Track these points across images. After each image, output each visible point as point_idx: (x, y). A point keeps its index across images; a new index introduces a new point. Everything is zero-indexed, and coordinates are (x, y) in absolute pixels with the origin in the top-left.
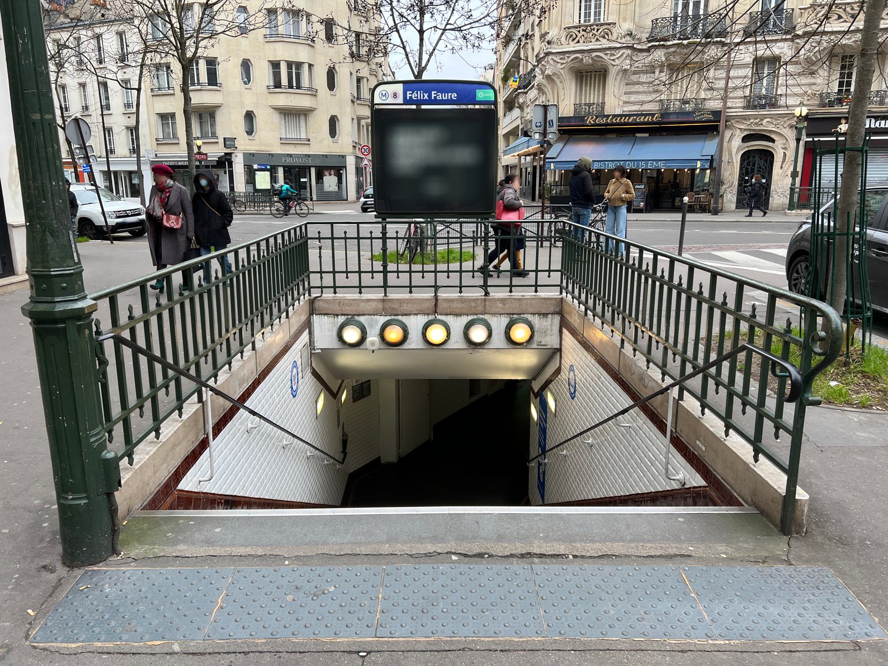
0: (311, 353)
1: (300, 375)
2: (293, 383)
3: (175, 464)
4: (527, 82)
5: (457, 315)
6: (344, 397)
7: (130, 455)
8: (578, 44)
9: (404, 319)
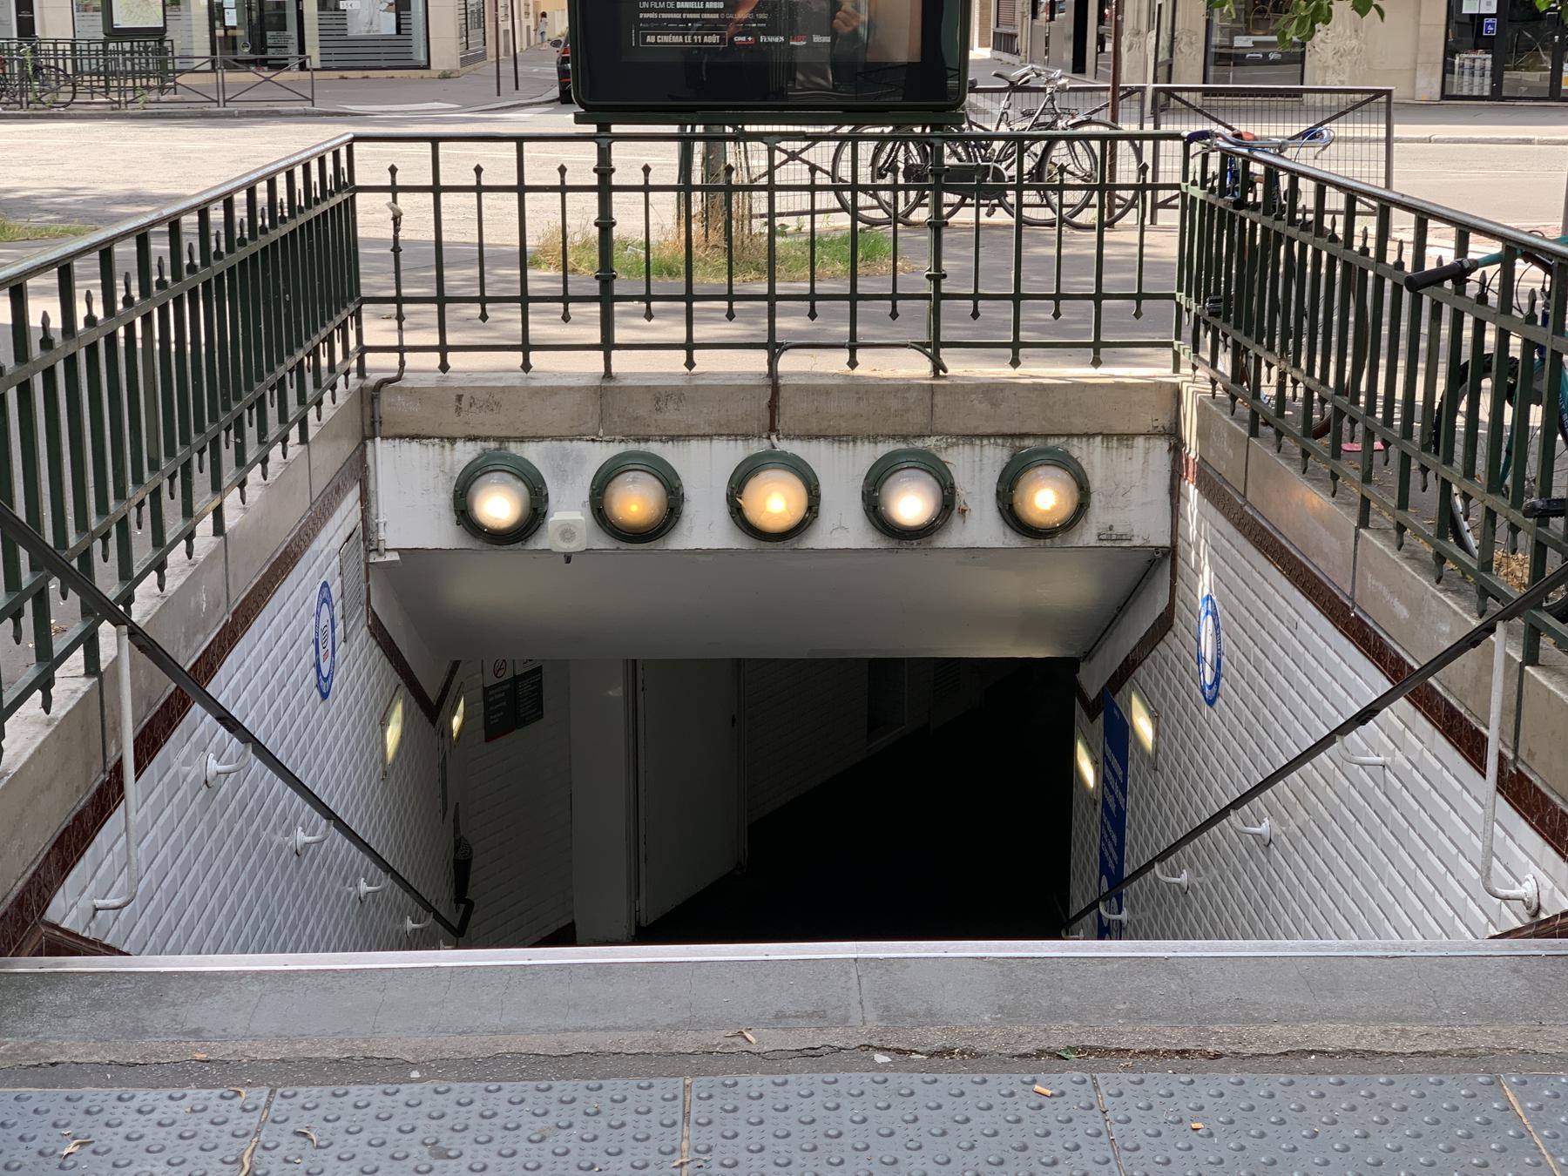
0: (367, 564)
2: (322, 651)
3: (39, 845)
5: (838, 438)
6: (456, 722)
9: (669, 453)
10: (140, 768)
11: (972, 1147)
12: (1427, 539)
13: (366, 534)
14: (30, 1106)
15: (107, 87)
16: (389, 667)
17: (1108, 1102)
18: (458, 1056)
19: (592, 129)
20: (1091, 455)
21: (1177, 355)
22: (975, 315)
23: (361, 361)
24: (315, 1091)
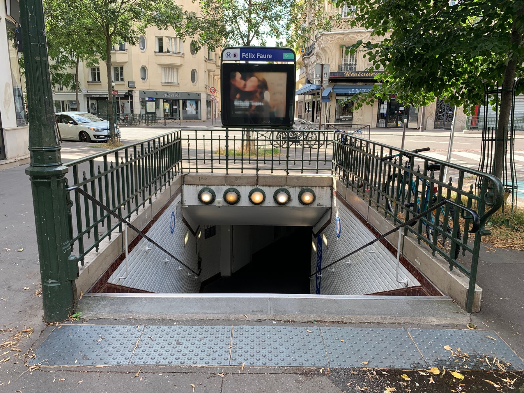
1: (176, 220)
4: (309, 51)
5: (269, 186)
6: (199, 236)
7: (82, 259)
8: (341, 30)
9: (238, 188)
10: (129, 252)
11: (294, 345)
12: (383, 209)
13: (182, 202)
14: (93, 329)
15: (145, 122)
16: (186, 227)
17: (323, 334)
18: (185, 319)
19: (225, 129)
20: (316, 190)
21: (332, 172)
22: (295, 164)
23: (182, 170)
24: (154, 327)
